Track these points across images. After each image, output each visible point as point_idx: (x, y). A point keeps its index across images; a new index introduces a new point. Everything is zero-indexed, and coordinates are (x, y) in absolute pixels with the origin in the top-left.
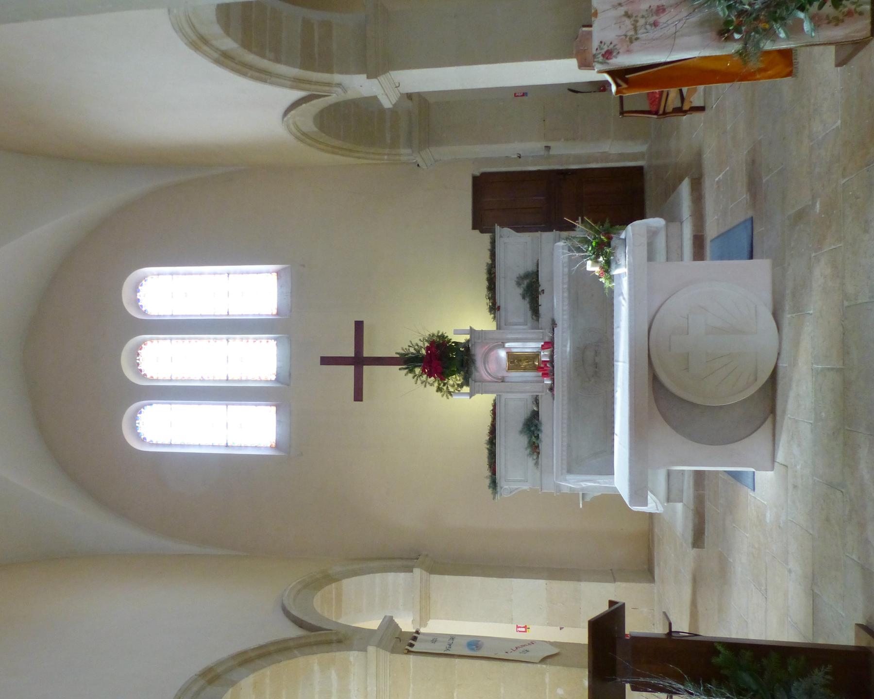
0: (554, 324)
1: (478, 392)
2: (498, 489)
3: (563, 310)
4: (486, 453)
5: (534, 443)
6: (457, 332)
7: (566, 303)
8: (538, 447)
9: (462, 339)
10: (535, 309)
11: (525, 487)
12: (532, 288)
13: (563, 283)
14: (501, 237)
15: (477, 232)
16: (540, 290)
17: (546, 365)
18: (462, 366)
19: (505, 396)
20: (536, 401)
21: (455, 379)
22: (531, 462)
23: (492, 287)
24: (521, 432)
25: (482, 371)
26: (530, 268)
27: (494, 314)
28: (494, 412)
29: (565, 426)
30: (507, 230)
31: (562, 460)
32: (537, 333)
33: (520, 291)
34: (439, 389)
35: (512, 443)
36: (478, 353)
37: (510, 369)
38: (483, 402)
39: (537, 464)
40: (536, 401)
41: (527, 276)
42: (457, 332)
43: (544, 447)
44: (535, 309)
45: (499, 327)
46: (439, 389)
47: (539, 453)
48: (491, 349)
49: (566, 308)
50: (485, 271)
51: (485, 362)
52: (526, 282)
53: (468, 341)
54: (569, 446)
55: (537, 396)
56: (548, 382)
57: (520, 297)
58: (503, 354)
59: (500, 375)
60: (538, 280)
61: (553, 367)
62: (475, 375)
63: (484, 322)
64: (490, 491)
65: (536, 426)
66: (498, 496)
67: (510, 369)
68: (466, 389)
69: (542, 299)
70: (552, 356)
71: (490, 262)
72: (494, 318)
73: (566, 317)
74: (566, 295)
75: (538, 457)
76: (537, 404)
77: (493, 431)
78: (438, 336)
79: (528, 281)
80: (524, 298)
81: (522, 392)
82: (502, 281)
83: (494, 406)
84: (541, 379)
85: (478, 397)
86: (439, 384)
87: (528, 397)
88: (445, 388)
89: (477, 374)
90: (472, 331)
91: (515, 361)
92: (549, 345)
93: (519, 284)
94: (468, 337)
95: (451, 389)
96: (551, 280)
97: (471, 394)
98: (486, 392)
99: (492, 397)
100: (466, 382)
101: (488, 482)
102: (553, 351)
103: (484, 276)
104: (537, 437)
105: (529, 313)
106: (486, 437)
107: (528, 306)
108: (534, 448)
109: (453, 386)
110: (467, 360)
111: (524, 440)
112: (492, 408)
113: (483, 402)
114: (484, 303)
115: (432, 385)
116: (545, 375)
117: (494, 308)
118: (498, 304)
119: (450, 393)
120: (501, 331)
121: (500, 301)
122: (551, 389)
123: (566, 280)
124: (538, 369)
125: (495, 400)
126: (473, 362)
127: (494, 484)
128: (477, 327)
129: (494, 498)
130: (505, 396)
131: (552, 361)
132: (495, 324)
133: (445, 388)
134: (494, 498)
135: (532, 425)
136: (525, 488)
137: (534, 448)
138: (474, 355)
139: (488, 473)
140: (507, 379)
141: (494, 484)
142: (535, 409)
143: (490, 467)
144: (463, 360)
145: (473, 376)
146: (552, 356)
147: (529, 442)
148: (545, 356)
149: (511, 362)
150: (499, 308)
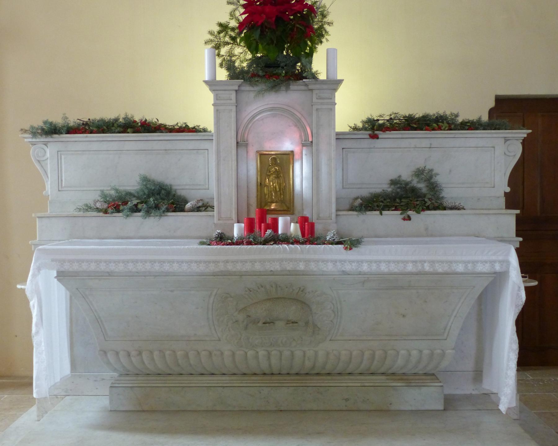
0: (351, 243)
1: (217, 98)
2: (44, 139)
3: (378, 262)
4: (109, 114)
5: (125, 203)
6: (331, 55)
7: (393, 268)
8: (117, 209)
9: (319, 64)
10: (373, 203)
11: (49, 188)
12: (412, 198)
13: (432, 262)
14: (506, 140)
15: (492, 104)
16: (410, 213)
17: (268, 227)
18: (268, 66)
19: (212, 147)
20: (204, 207)
21: (242, 55)
22: (92, 197)
23: (412, 124)
24: (145, 180)
25: (262, 103)
26: (449, 194)
27: (364, 129)
28: (184, 129)
29: (148, 266)
30: (516, 151)
31: (80, 261)
32: (329, 208)
33: (406, 174)
34: (224, 27)
35: (127, 163)
36: (292, 97)
37: (262, 155)
38: (199, 108)
39: (88, 208)
40: (204, 207)
41: (434, 187)
42: (331, 55)
43: (118, 221)
44: (373, 203)
45: (340, 137)
46: (224, 27)
47: (106, 212)
48: (299, 125)
49: (384, 268)
50: (441, 112)
51: (276, 111)
52: (422, 186)
53: (314, 76)
54: (110, 274)
55: (212, 207)
56: (238, 230)
57: (394, 176)
58: (287, 146)
59: (251, 139)
60: (428, 209)
61: (265, 242)
62: (250, 92)
63: (349, 109)
64: (38, 123)
65: (157, 207)
66: (28, 138)
67: (262, 155)
68: (222, 75)
69: (391, 218)
70: (286, 240)
71: (460, 120)
72: (355, 129)
73: (365, 268)
74: (410, 268)
75: (98, 210)
76: (198, 209)
77: (147, 127)
78: (321, 27)
79: (424, 190)
80: (393, 182)
81: (218, 180)
82: (425, 143)
83: (194, 130)
84: (244, 217)
85: (208, 97)
86: (233, 29)
87: (211, 191)
88: (227, 39)
89: (252, 95)
90: (334, 84)
91: (277, 166)
92: (309, 235)
93: (419, 173)
94: (322, 77)
95: (224, 51)
96: (429, 234)
97: (212, 84)
98: (217, 112)
99: (211, 127)
100: (235, 74)
101: (58, 120)
102: (296, 242)
103: (432, 109)
104: (135, 209)
105: (365, 193)
106: (151, 117)
107: (378, 191)
108: (117, 204)
109: (231, 55)
110: (277, 76)
111: (131, 184)
112: (191, 126)
113: (199, 108)
114: (382, 111)
115: (232, 15)
116: (250, 226)
117: (374, 128)
118: (381, 134)
119: (217, 47)
120: (333, 141)
121: (388, 140)
122: (222, 239)
123: (439, 269)
124: (263, 213)
125: (205, 130)
126: (275, 88)
127: (52, 130)
128: (340, 96)
129: (24, 131)
130: (212, 147)
131: (276, 240)
132: (347, 129)
133: (227, 39)
134: (24, 131)
135: (160, 199)
136: (48, 186)
137: (117, 204)
138: (288, 89)
139: (73, 120)
140: (242, 151)
141: (52, 130)
142: (188, 206)
143: (86, 124)
144: (278, 66)
145: (247, 88)
146: (286, 240)
147: (130, 194)
148: (286, 225)
149: (274, 159)
150: (374, 137)
